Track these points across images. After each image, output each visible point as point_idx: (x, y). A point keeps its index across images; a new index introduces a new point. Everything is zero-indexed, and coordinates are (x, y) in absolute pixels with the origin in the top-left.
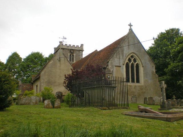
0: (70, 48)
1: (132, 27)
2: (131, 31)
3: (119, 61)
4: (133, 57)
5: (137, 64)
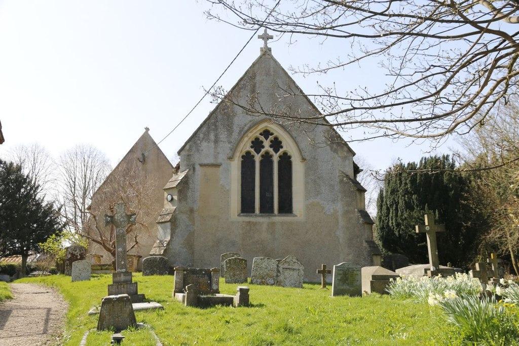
1: (270, 40)
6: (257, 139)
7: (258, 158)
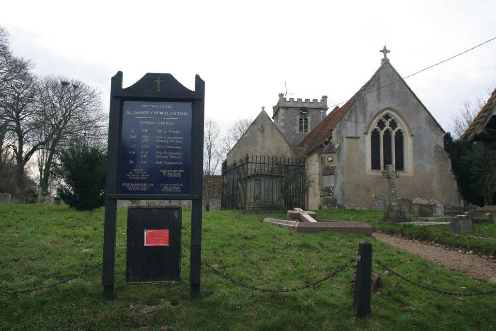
0: (299, 105)
2: (385, 63)
3: (356, 126)
4: (390, 118)
5: (399, 130)
6: (381, 120)
7: (382, 133)
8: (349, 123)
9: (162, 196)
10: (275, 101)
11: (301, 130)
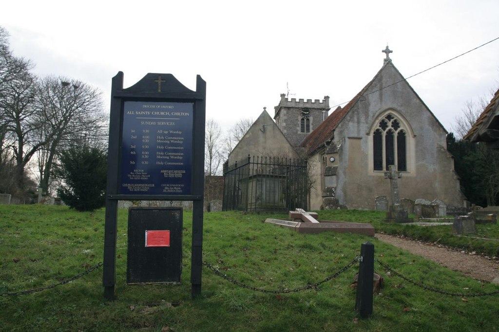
0: (301, 106)
2: (388, 64)
3: (358, 127)
4: (393, 118)
5: (402, 131)
6: (383, 121)
7: (384, 134)
8: (351, 124)
9: (163, 196)
10: (277, 102)
11: (303, 131)
